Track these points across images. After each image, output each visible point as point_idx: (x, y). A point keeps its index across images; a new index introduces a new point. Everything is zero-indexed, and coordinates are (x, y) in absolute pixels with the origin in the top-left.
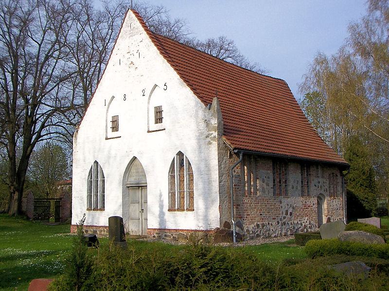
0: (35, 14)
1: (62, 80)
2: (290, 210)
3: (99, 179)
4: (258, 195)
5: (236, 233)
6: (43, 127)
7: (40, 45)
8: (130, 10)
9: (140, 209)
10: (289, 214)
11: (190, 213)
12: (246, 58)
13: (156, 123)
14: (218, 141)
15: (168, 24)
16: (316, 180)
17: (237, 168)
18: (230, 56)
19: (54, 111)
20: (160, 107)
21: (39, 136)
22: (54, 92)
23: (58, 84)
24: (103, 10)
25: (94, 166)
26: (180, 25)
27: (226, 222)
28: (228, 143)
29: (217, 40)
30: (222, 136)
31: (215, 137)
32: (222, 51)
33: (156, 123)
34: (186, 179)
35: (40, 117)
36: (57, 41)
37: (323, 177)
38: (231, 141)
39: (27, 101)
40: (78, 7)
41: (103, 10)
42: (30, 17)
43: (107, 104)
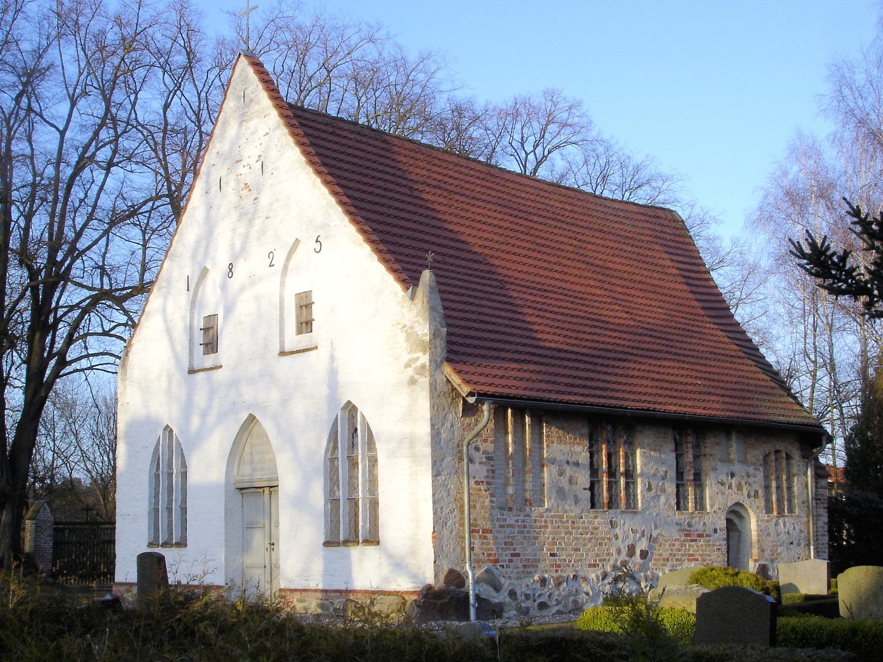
0: (52, 55)
1: (116, 220)
2: (642, 545)
3: (175, 471)
4: (546, 506)
5: (477, 597)
6: (70, 340)
7: (62, 133)
8: (242, 57)
9: (267, 541)
10: (638, 553)
11: (371, 550)
12: (616, 149)
13: (300, 332)
14: (431, 376)
15: (399, 64)
16: (723, 469)
17: (485, 441)
18: (573, 139)
19: (95, 301)
20: (308, 294)
21: (63, 363)
22: (94, 255)
23: (106, 232)
24: (229, 34)
25: (164, 438)
26: (433, 68)
27: (451, 571)
28: (456, 380)
29: (537, 100)
30: (442, 362)
31: (423, 367)
32: (552, 128)
33: (300, 332)
34: (363, 470)
35: (65, 314)
36: (108, 119)
37: (744, 462)
38: (465, 376)
39: (33, 274)
40: (160, 37)
41: (229, 34)
42: (44, 63)
43: (192, 288)
